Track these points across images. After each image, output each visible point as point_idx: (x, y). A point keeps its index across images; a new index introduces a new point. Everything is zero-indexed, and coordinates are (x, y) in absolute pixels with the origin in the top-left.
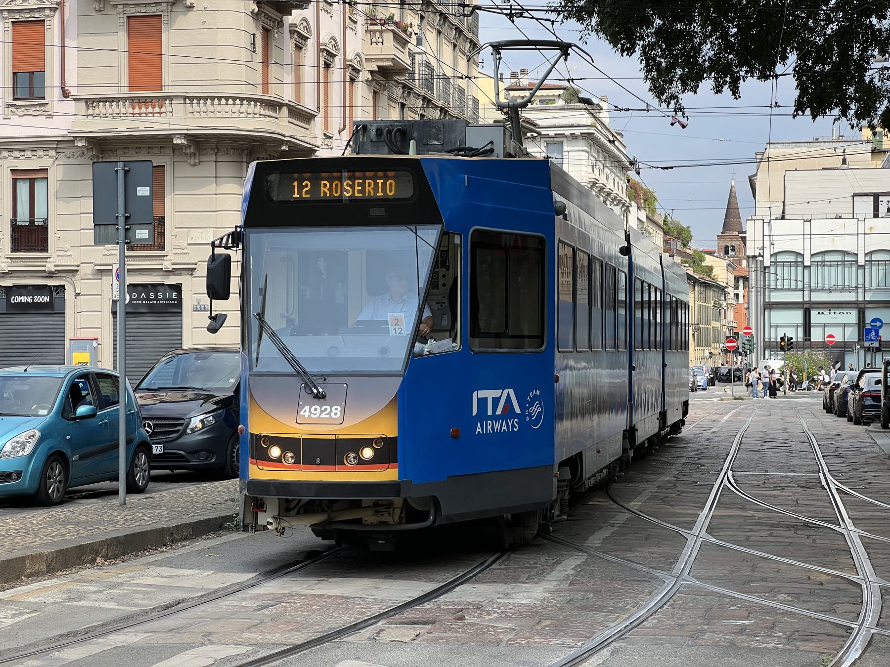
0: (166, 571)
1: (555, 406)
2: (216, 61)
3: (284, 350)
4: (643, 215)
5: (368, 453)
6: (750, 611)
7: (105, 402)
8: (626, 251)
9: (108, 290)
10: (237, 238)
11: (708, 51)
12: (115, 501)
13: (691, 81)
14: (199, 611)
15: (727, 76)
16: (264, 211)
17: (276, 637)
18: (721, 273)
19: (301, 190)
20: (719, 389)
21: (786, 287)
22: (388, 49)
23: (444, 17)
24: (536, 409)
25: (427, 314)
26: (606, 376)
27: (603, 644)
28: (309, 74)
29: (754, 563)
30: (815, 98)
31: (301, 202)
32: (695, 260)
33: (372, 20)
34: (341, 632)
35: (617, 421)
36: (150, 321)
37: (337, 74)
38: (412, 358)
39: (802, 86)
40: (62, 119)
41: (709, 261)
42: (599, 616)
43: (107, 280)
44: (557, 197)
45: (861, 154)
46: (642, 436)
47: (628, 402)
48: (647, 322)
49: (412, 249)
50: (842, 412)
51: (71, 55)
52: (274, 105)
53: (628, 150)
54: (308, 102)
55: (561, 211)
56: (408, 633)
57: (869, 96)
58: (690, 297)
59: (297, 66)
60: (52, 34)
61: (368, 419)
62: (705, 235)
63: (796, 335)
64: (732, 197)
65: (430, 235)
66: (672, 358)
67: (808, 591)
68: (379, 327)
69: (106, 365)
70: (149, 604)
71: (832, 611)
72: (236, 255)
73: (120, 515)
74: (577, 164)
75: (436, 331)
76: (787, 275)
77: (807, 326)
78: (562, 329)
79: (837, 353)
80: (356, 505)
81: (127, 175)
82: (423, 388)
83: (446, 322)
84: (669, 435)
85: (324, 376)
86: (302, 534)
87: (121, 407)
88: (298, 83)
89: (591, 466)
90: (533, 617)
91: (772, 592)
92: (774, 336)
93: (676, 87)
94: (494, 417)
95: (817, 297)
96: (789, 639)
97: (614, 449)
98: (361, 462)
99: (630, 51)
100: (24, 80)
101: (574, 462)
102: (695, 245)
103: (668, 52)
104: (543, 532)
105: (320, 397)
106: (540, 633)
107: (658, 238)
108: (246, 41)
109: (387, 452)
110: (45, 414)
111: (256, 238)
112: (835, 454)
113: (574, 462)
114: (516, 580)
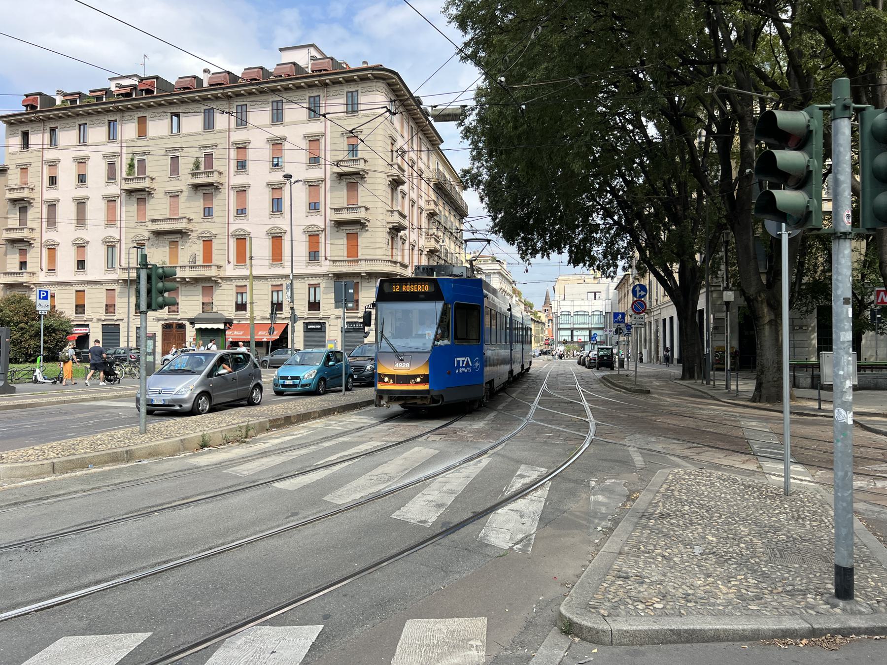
0: (358, 417)
1: (484, 362)
2: (376, 248)
3: (390, 344)
4: (517, 299)
5: (418, 380)
6: (552, 431)
7: (338, 361)
8: (510, 310)
9: (339, 324)
10: (374, 305)
11: (539, 245)
12: (341, 394)
13: (534, 253)
14: (368, 430)
15: (545, 252)
16: (383, 296)
17: (394, 439)
18: (544, 318)
19: (396, 289)
20: (542, 357)
21: (565, 322)
22: (433, 244)
23: (451, 233)
24: (477, 364)
25: (440, 331)
26: (504, 353)
27: (503, 442)
28: (406, 252)
29: (553, 415)
30: (576, 260)
31: (396, 292)
32: (535, 314)
33: (428, 234)
34: (415, 438)
35: (507, 368)
36: (354, 334)
37: (416, 252)
38: (434, 346)
39: (570, 256)
40: (325, 267)
41: (539, 314)
42: (502, 433)
43: (339, 320)
44: (485, 291)
45: (590, 278)
46: (515, 373)
47: (510, 361)
48: (517, 334)
49: (436, 308)
50: (584, 365)
51: (328, 246)
52: (395, 262)
53: (511, 278)
54: (406, 262)
55: (486, 296)
56: (439, 437)
57: (593, 260)
58: (533, 326)
59: (403, 250)
60: (322, 240)
61: (421, 369)
62: (538, 306)
63: (569, 339)
64: (547, 293)
65: (440, 305)
66: (526, 347)
67: (570, 424)
68: (423, 336)
69: (339, 349)
70: (352, 428)
71: (579, 431)
72: (373, 311)
73: (343, 398)
74: (495, 282)
75: (442, 337)
76: (565, 319)
77: (572, 336)
78: (486, 337)
79: (583, 345)
80: (415, 398)
81: (345, 285)
82: (438, 358)
83: (446, 334)
84: (525, 373)
85: (403, 353)
86: (396, 407)
87: (343, 362)
88: (403, 255)
89: (497, 384)
90: (479, 432)
91: (559, 425)
92: (561, 339)
93: (529, 256)
94: (463, 367)
95: (575, 326)
96: (565, 440)
97: (506, 377)
98: (416, 383)
99: (513, 244)
100: (312, 254)
101: (491, 382)
102: (534, 309)
103: (525, 245)
104: (480, 406)
105: (402, 360)
106: (482, 438)
107: (522, 306)
108: (385, 241)
109: (425, 379)
110: (319, 365)
111: (380, 305)
112: (581, 378)
113: (491, 382)
114: (473, 420)
